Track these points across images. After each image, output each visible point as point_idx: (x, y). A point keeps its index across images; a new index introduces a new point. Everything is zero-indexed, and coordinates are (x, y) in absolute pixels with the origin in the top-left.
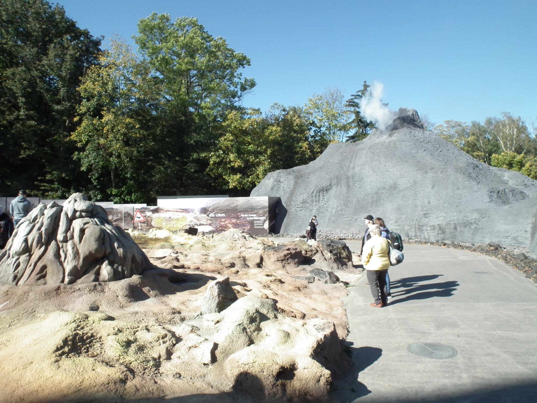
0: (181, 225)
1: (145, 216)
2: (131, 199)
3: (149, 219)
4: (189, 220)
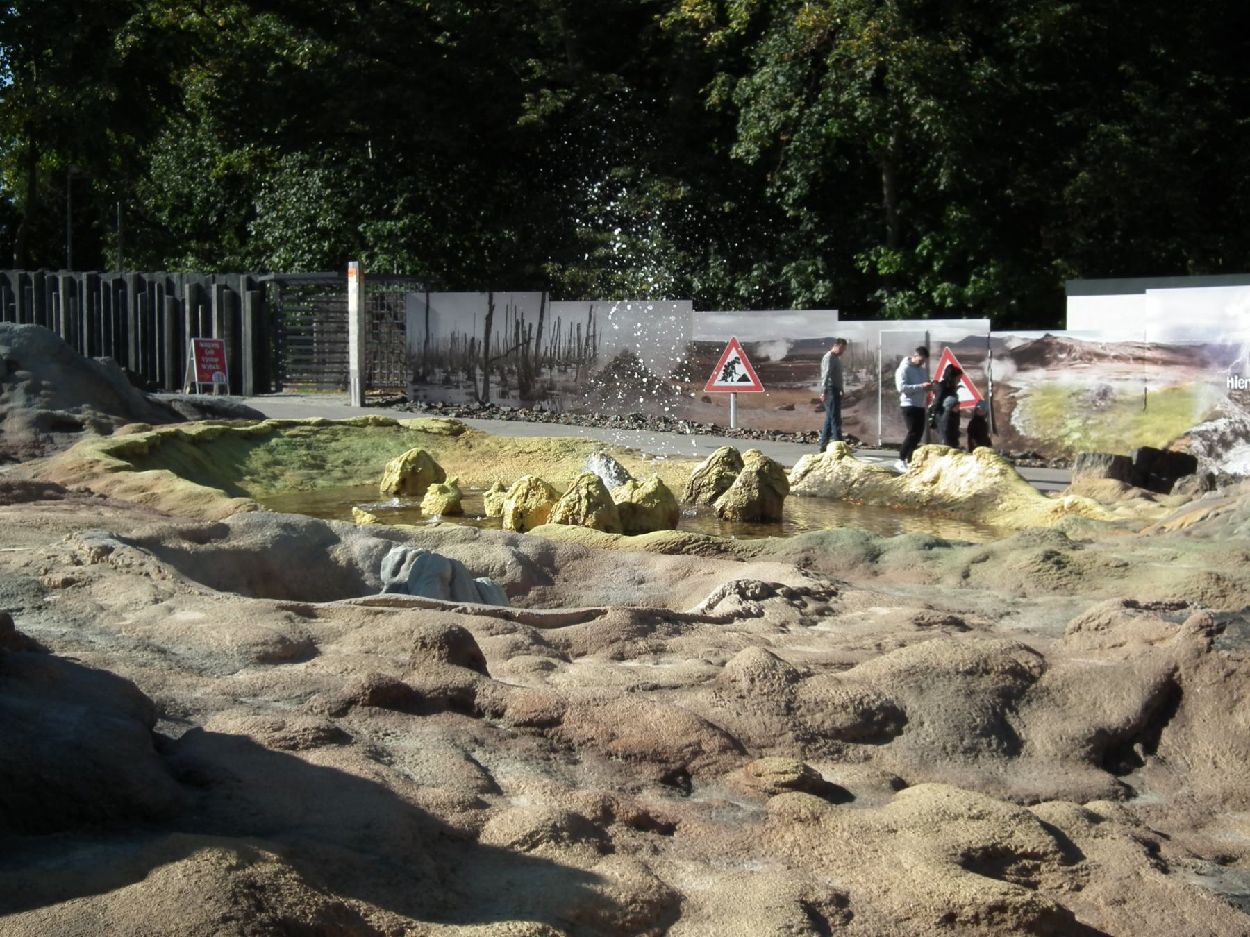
0: (1159, 431)
1: (983, 383)
2: (958, 296)
3: (1000, 397)
4: (1203, 406)
